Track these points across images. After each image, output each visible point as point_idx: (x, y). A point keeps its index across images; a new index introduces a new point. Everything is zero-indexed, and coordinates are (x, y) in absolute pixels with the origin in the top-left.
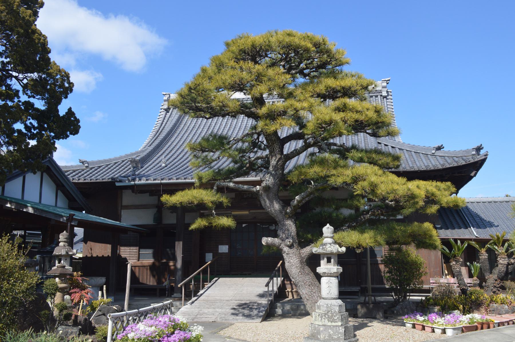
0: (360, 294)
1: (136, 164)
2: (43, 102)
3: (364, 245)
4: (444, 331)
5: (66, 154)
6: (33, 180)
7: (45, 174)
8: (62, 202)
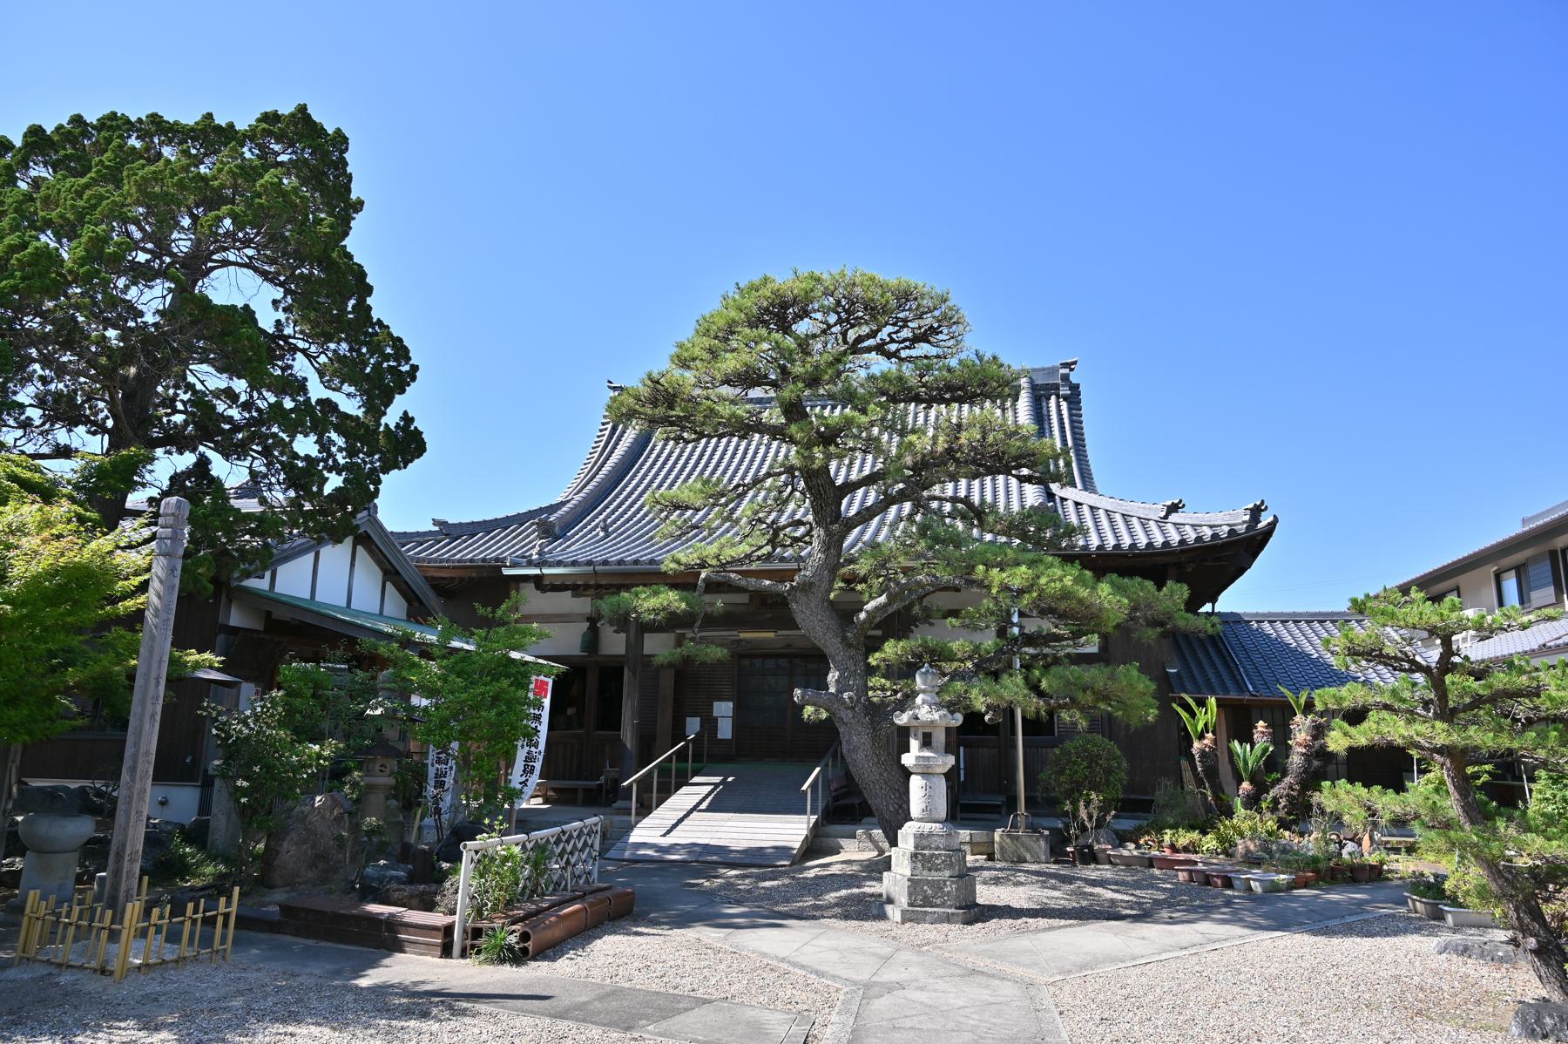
0: (1004, 810)
2: (357, 401)
5: (402, 504)
6: (335, 556)
7: (359, 548)
8: (395, 604)
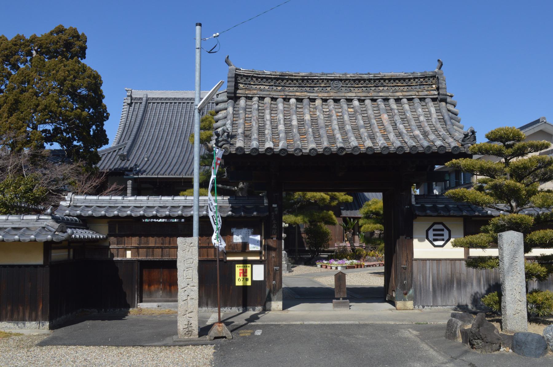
1: (124, 158)
3: (298, 223)
4: (337, 268)
